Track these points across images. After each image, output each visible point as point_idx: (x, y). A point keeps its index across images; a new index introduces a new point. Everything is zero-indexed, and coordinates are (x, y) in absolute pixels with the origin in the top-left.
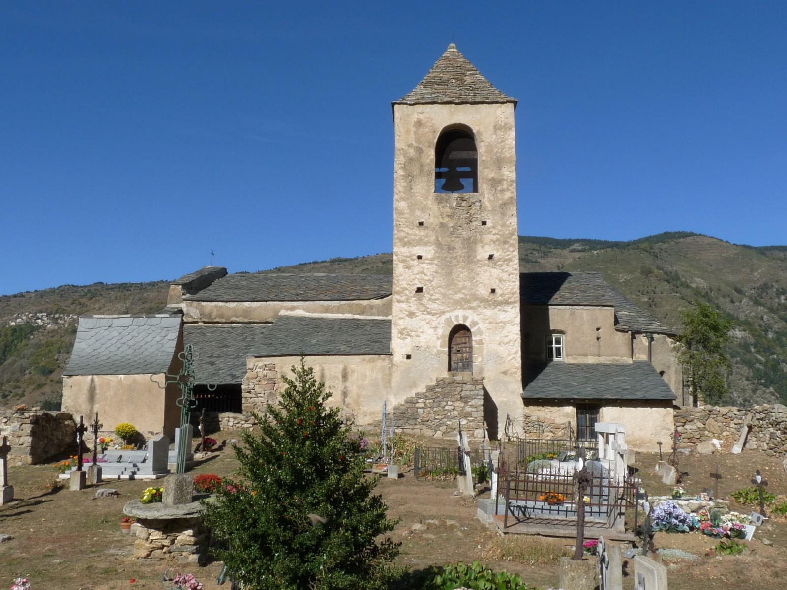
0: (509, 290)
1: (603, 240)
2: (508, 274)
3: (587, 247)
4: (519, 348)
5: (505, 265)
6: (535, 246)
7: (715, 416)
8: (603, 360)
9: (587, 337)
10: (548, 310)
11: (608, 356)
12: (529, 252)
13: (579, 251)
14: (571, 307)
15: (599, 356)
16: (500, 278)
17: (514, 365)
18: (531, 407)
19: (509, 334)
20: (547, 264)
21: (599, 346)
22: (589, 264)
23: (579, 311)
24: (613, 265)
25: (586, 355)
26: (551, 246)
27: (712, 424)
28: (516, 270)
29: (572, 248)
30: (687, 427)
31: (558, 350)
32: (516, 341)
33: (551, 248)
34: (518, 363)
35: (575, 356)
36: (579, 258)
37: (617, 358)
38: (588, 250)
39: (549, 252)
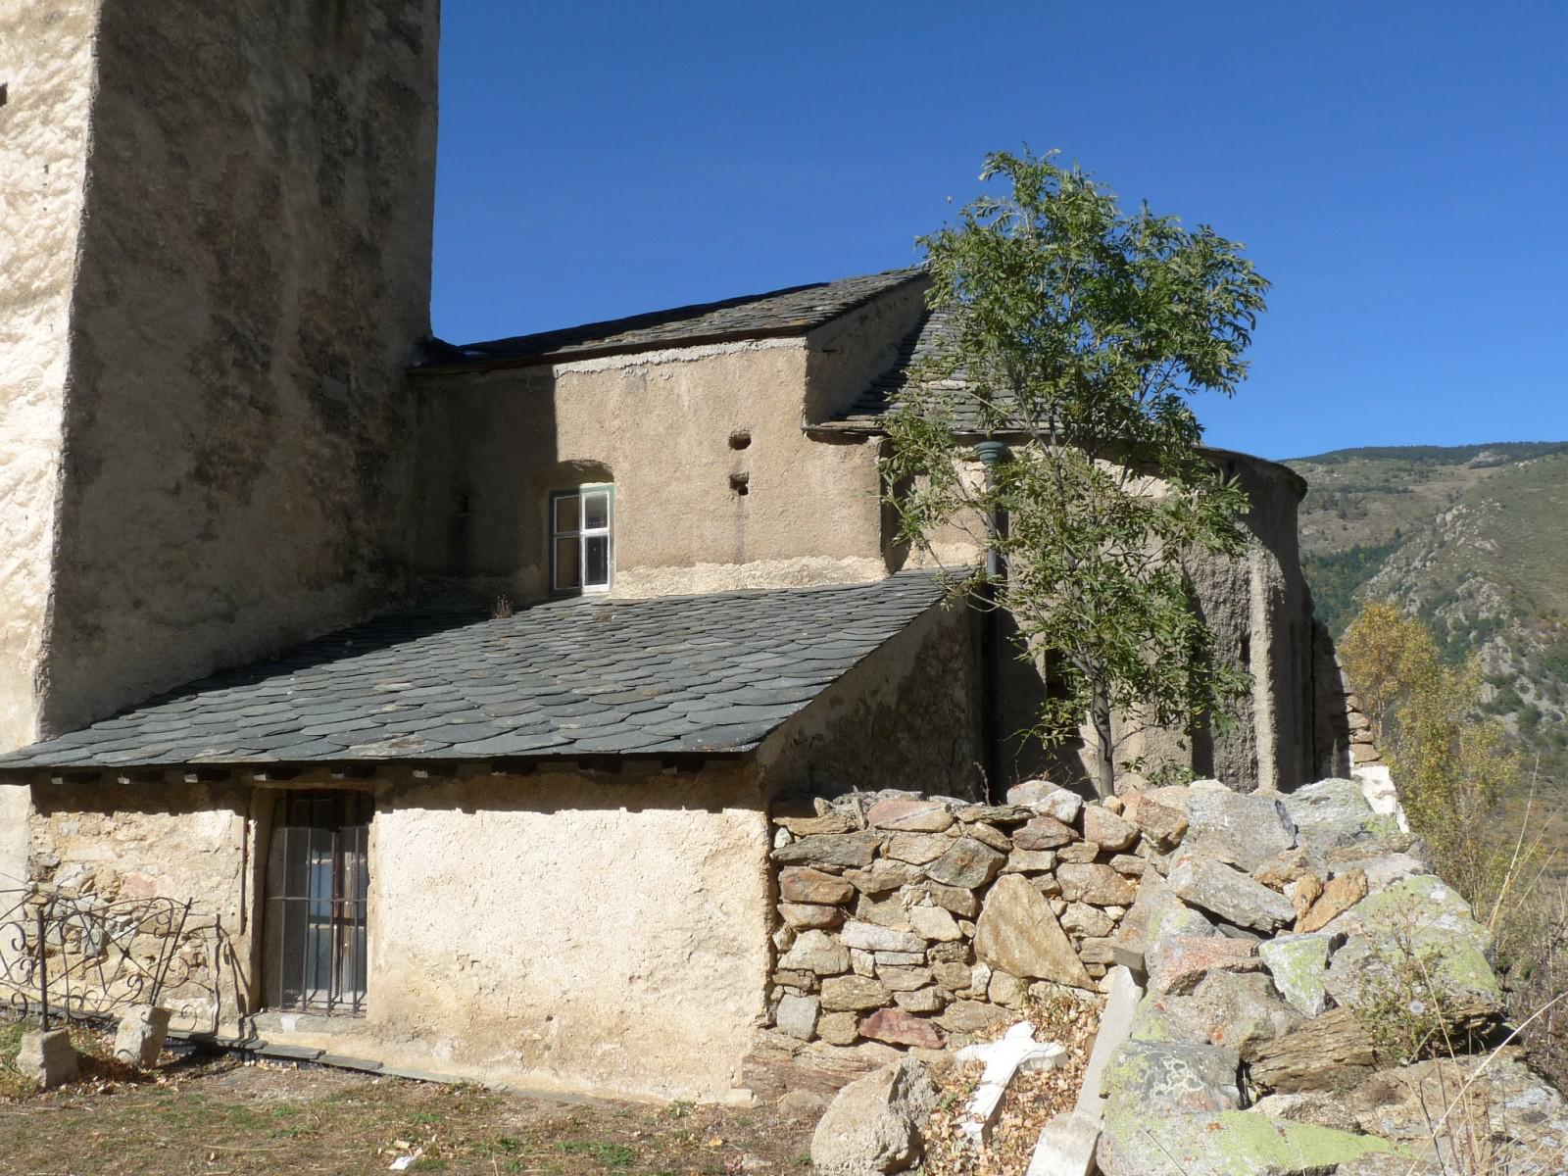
0: (40, 233)
1: (1536, 441)
2: (41, 161)
3: (1506, 456)
4: (50, 515)
5: (36, 125)
6: (1402, 463)
7: (1045, 860)
8: (761, 575)
9: (688, 479)
10: (550, 381)
11: (779, 556)
12: (1391, 474)
13: (1489, 465)
14: (629, 359)
15: (739, 559)
16: (15, 185)
17: (20, 603)
18: (66, 821)
19: (16, 447)
20: (1427, 494)
21: (740, 516)
22: (1510, 487)
23: (665, 369)
24: (1557, 486)
25: (685, 561)
26: (1434, 460)
27: (1019, 913)
28: (73, 134)
29: (1475, 460)
30: (854, 932)
31: (598, 546)
32: (41, 475)
33: (1433, 465)
34: (37, 589)
35: (641, 570)
36: (1490, 477)
37: (815, 563)
38: (1508, 461)
39: (1431, 471)
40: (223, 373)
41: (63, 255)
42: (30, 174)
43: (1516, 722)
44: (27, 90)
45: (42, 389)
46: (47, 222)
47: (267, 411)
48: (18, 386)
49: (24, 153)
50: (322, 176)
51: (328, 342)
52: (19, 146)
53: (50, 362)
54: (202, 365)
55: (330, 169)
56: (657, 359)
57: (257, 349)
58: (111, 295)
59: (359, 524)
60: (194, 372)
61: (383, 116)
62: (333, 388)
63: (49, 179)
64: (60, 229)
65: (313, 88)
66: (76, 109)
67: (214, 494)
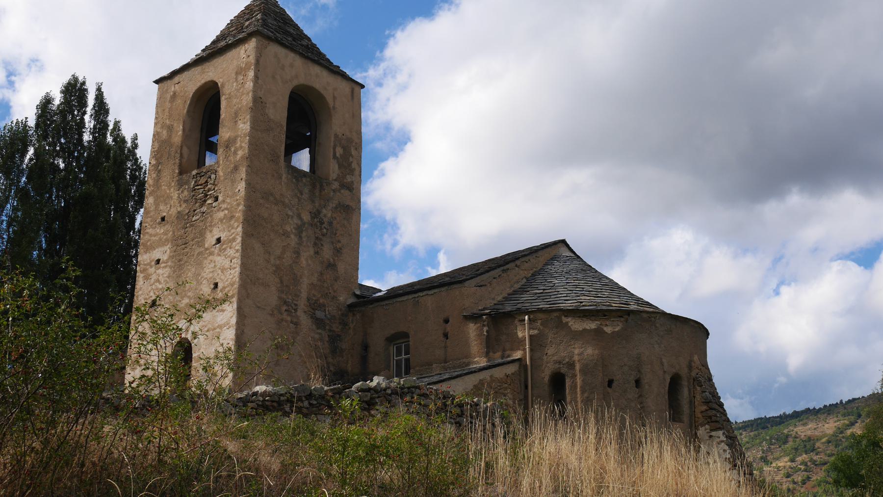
0: (230, 280)
16: (223, 266)
21: (445, 347)
23: (424, 298)
40: (281, 314)
41: (235, 286)
42: (227, 263)
43: (765, 416)
44: (226, 238)
45: (230, 324)
46: (231, 277)
47: (296, 324)
48: (224, 324)
49: (225, 257)
50: (315, 244)
51: (318, 300)
52: (224, 255)
53: (232, 317)
54: (275, 312)
55: (317, 243)
56: (422, 295)
57: (293, 305)
58: (248, 296)
59: (330, 360)
60: (272, 315)
61: (338, 218)
62: (319, 314)
63: (232, 264)
64: (234, 279)
65: (311, 216)
66: (237, 245)
67: (279, 352)
